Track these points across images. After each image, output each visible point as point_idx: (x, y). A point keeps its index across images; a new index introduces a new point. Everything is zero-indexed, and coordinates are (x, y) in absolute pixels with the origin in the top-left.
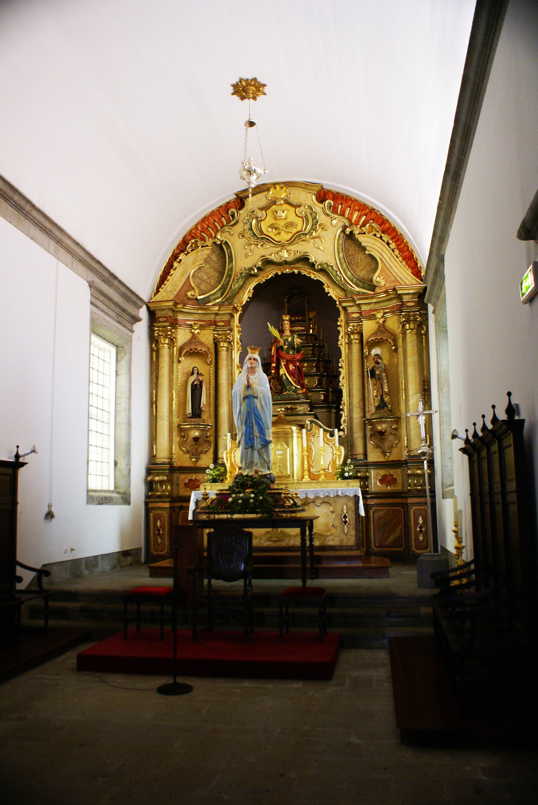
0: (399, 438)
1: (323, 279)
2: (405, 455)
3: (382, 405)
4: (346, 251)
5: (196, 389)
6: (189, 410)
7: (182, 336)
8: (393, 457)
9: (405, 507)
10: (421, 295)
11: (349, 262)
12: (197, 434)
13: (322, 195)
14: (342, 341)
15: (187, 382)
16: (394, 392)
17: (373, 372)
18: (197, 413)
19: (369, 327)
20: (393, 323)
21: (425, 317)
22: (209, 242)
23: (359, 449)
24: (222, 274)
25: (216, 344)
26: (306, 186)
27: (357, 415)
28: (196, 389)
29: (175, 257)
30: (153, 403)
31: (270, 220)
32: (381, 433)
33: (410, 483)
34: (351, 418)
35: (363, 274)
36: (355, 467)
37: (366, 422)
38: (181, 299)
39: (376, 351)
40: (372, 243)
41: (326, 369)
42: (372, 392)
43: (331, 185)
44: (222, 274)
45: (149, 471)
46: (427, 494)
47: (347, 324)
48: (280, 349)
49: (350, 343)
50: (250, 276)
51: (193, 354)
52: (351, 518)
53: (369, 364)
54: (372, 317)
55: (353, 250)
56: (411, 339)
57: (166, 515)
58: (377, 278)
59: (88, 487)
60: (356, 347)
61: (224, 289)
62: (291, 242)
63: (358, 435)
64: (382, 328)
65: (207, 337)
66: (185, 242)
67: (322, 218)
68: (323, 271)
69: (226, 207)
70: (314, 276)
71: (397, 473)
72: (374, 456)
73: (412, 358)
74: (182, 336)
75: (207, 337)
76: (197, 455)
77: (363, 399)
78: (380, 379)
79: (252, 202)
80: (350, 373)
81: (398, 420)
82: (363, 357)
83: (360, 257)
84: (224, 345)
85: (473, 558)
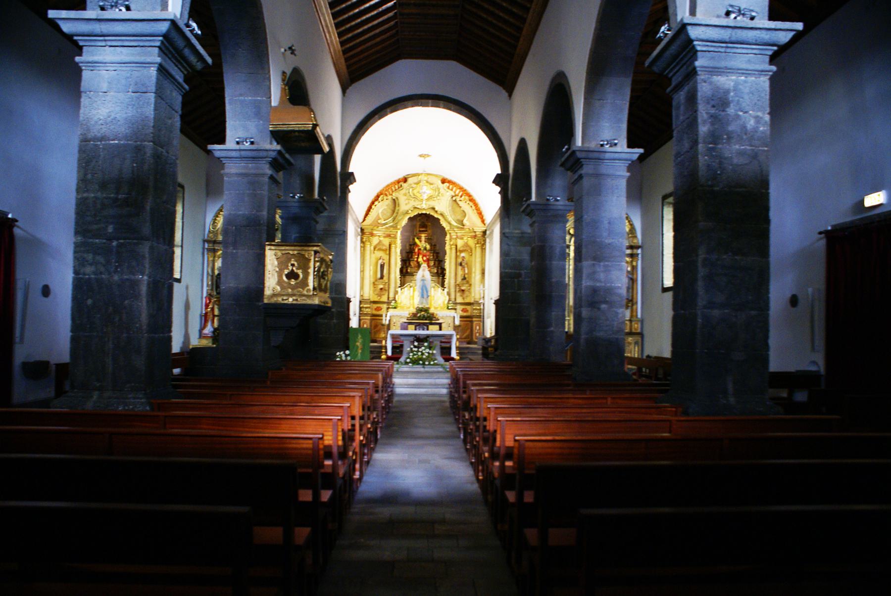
0: (470, 292)
1: (440, 217)
2: (472, 301)
3: (464, 279)
4: (453, 208)
5: (382, 266)
6: (379, 276)
7: (375, 241)
8: (467, 301)
9: (472, 322)
10: (484, 233)
11: (454, 212)
12: (382, 286)
13: (444, 181)
14: (447, 248)
15: (377, 263)
16: (470, 273)
17: (461, 264)
18: (382, 277)
19: (460, 243)
20: (471, 242)
21: (485, 241)
22: (390, 197)
23: (453, 297)
24: (394, 211)
25: (390, 245)
26: (436, 176)
27: (453, 282)
28: (382, 266)
29: (373, 203)
30: (362, 271)
31: (418, 189)
32: (463, 291)
33: (326, 487)
34: (449, 283)
35: (459, 217)
36: (452, 305)
37: (456, 285)
38: (376, 224)
39: (463, 254)
40: (465, 206)
41: (437, 257)
42: (460, 272)
43: (449, 177)
44: (394, 211)
45: (360, 302)
46: (481, 317)
47: (450, 240)
48: (419, 249)
49: (451, 249)
50: (407, 213)
51: (380, 250)
52: (452, 325)
53: (460, 260)
54: (462, 239)
55: (455, 205)
56: (478, 250)
57: (368, 322)
58: (465, 222)
59: (663, 284)
60: (454, 251)
61: (394, 219)
62: (428, 200)
63: (452, 290)
64: (466, 245)
65: (386, 242)
66: (378, 196)
67: (442, 191)
68: (441, 214)
69: (399, 182)
70: (436, 216)
71: (468, 308)
72: (459, 300)
73: (478, 259)
74: (375, 241)
75: (386, 242)
76: (380, 295)
77: (456, 274)
78: (464, 267)
79: (410, 180)
80: (450, 262)
81: (470, 285)
82: (457, 257)
83: (458, 209)
84: (393, 246)
85: (493, 334)
